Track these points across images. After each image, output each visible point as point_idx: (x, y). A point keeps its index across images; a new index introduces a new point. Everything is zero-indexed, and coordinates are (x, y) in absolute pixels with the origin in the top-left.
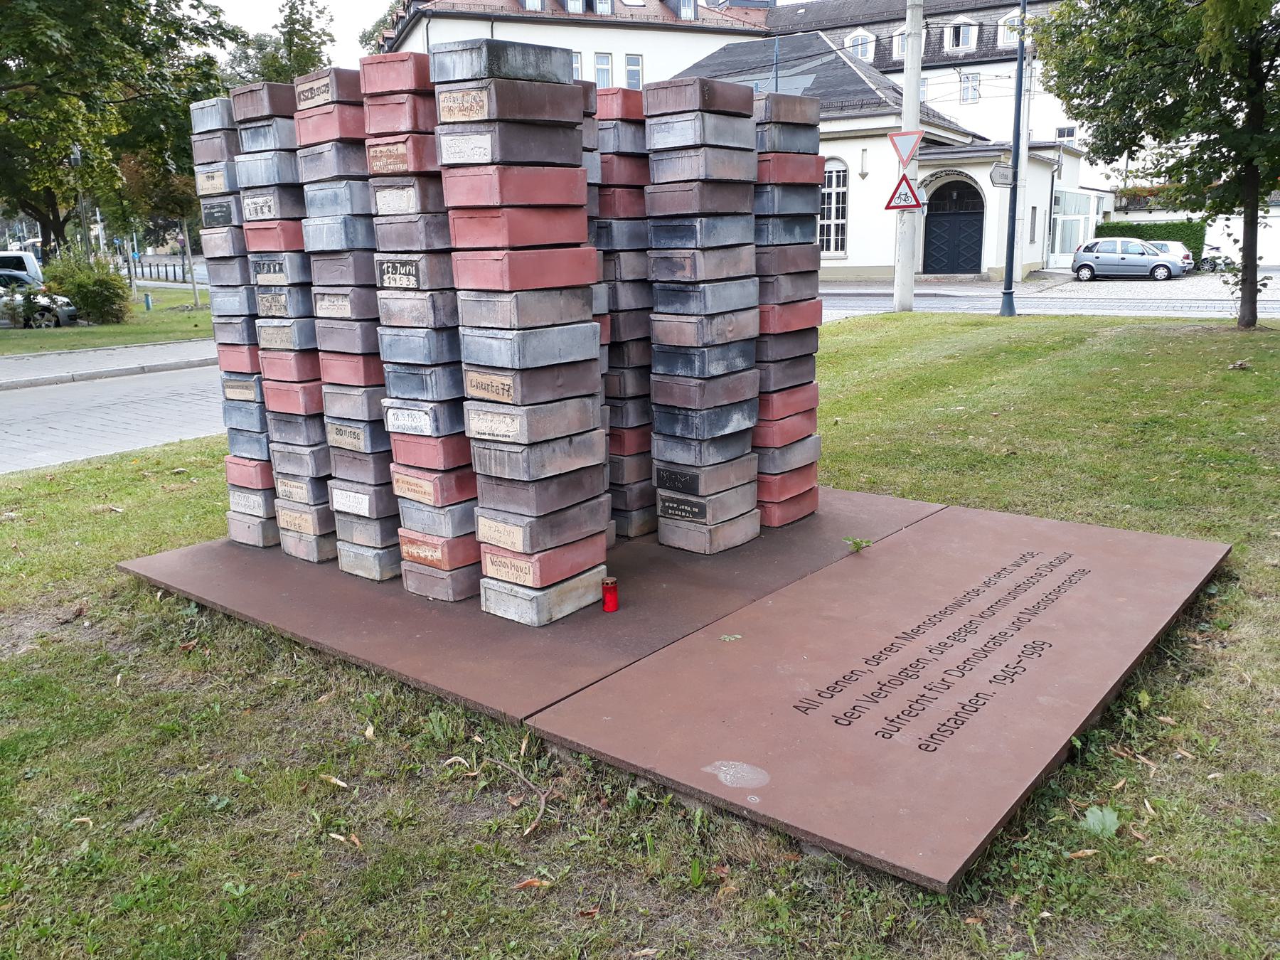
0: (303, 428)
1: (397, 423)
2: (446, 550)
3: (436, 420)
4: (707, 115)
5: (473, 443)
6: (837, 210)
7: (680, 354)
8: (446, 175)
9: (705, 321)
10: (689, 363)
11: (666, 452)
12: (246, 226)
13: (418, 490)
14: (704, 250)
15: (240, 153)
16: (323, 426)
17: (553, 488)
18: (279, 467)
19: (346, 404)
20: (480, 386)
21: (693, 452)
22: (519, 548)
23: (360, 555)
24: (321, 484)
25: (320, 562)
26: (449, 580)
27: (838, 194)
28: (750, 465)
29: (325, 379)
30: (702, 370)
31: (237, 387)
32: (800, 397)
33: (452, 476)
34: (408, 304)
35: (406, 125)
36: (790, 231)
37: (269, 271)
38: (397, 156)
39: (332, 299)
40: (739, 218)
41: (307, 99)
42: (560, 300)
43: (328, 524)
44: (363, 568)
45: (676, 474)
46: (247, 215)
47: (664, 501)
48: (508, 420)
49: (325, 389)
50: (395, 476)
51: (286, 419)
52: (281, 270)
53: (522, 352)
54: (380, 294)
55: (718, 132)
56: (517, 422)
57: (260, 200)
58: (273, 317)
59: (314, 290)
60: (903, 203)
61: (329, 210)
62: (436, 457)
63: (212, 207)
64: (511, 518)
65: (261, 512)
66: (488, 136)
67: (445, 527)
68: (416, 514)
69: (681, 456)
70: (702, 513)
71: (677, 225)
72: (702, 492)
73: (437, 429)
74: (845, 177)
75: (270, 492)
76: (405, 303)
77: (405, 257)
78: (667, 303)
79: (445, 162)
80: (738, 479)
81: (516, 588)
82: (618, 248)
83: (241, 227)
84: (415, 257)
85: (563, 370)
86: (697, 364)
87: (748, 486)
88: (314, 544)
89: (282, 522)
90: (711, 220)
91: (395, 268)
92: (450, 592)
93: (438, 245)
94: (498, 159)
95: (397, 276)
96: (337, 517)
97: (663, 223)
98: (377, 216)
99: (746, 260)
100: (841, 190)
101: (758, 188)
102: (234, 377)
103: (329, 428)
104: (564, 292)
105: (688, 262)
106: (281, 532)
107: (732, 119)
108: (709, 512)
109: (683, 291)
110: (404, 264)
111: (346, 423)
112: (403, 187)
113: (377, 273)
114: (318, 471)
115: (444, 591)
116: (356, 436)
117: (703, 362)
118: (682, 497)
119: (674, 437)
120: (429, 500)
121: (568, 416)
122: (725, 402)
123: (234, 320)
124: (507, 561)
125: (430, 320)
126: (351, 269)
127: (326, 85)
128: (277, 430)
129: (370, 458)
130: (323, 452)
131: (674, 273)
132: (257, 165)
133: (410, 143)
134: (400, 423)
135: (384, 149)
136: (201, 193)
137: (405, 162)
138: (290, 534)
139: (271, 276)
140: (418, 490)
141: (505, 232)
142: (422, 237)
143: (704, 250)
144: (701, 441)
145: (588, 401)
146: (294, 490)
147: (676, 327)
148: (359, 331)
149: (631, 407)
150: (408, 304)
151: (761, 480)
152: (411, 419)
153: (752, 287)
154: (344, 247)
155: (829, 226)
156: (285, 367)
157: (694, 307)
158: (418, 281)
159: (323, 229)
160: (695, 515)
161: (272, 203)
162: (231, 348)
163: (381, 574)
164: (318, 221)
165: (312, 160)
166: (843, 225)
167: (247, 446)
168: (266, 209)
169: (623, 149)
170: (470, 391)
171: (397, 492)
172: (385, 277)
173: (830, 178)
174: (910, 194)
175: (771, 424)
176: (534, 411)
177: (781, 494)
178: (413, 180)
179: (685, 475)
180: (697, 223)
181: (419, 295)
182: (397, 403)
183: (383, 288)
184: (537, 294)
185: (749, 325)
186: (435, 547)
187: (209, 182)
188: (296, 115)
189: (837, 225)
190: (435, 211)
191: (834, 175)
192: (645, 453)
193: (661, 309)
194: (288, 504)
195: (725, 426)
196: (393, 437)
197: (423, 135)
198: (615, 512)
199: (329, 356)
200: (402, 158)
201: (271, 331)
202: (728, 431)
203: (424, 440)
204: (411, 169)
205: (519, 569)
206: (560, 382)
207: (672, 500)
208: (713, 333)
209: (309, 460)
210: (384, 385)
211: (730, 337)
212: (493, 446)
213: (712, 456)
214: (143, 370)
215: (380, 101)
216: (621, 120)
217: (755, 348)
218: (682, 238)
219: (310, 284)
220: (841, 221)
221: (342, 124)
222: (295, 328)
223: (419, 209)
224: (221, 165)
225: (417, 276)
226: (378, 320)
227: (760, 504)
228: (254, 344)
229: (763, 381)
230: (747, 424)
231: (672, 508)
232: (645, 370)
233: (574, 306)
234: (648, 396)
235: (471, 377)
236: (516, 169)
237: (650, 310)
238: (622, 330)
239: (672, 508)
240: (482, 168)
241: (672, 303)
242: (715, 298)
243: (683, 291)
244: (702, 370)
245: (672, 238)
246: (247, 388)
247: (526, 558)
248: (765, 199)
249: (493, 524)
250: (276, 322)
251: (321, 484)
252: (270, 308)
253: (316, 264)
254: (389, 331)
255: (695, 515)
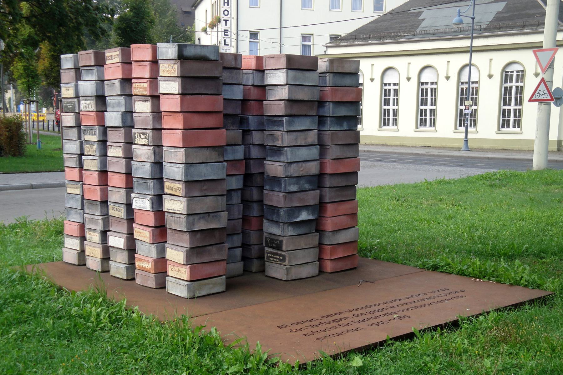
0: (99, 207)
1: (137, 205)
2: (153, 263)
3: (152, 203)
4: (289, 71)
5: (166, 214)
6: (516, 98)
7: (276, 180)
8: (161, 97)
9: (287, 165)
10: (280, 184)
11: (270, 229)
12: (81, 113)
13: (143, 235)
14: (287, 132)
15: (81, 80)
16: (108, 206)
17: (199, 235)
18: (88, 226)
19: (117, 196)
20: (170, 188)
21: (280, 229)
22: (182, 262)
23: (118, 268)
24: (104, 234)
25: (102, 272)
26: (154, 278)
27: (517, 87)
28: (314, 239)
29: (110, 184)
30: (285, 189)
31: (73, 188)
32: (345, 208)
33: (158, 229)
34: (144, 151)
35: (148, 76)
36: (341, 125)
37: (90, 134)
38: (144, 88)
39: (115, 148)
40: (308, 117)
41: (110, 59)
42: (207, 152)
43: (106, 250)
44: (119, 273)
45: (272, 239)
46: (82, 108)
47: (268, 253)
48: (179, 203)
49: (109, 189)
50: (135, 229)
51: (92, 202)
52: (95, 134)
53: (186, 173)
54: (134, 147)
55: (295, 78)
56: (183, 205)
57: (88, 102)
58: (90, 155)
59: (108, 144)
60: (541, 98)
61: (116, 109)
62: (151, 221)
63: (67, 103)
64: (179, 248)
65: (78, 248)
66: (177, 83)
67: (154, 254)
68: (142, 246)
69: (276, 230)
70: (284, 260)
71: (275, 120)
72: (284, 248)
73: (153, 207)
74: (522, 75)
75: (83, 238)
76: (143, 152)
77: (144, 131)
78: (271, 157)
79: (161, 92)
80: (306, 245)
81: (180, 281)
82: (252, 129)
83: (79, 113)
84: (148, 131)
85: (206, 183)
86: (283, 185)
87: (312, 249)
88: (100, 262)
89: (87, 253)
90: (291, 118)
91: (140, 136)
92: (154, 283)
93: (158, 127)
94: (180, 92)
95: (141, 139)
96: (111, 249)
97: (271, 118)
98: (135, 112)
99: (312, 137)
100: (520, 84)
101: (321, 103)
102: (71, 183)
103: (110, 207)
104: (209, 149)
105: (280, 137)
106: (86, 257)
107: (304, 72)
108: (287, 259)
109: (278, 150)
110: (144, 134)
111: (117, 205)
112: (146, 101)
113: (133, 137)
114: (104, 228)
115: (152, 284)
116: (120, 211)
117: (285, 185)
118: (276, 251)
119: (272, 221)
120: (148, 240)
121: (207, 204)
122: (298, 205)
123: (74, 156)
124: (177, 268)
125: (152, 159)
126: (123, 135)
127: (118, 55)
128: (89, 208)
129: (125, 221)
130: (106, 217)
131: (274, 142)
132: (88, 87)
133: (148, 83)
134: (138, 205)
135: (139, 84)
136: (63, 96)
137: (146, 91)
138: (90, 258)
139: (90, 136)
140: (143, 235)
141: (182, 122)
142: (151, 123)
143: (287, 132)
144: (285, 223)
145: (219, 198)
146: (93, 237)
147: (274, 168)
148: (124, 163)
149: (255, 206)
150: (144, 151)
151: (321, 246)
152: (142, 204)
153: (314, 152)
154: (121, 126)
155: (509, 110)
156: (92, 179)
157: (282, 158)
158: (148, 142)
159: (113, 118)
160: (281, 260)
161: (92, 104)
162: (71, 169)
163: (127, 276)
164: (111, 113)
165: (110, 86)
166: (520, 110)
167: (75, 216)
168: (90, 106)
169: (256, 84)
170: (167, 191)
171: (135, 237)
172: (136, 139)
173: (512, 76)
174: (546, 92)
175: (327, 219)
176: (190, 200)
177: (331, 255)
178: (149, 98)
179: (277, 240)
180: (284, 119)
181: (149, 148)
182: (137, 195)
183: (135, 144)
184: (195, 149)
185: (313, 168)
186: (148, 262)
187: (67, 91)
188: (105, 66)
189: (515, 110)
190: (157, 113)
191: (515, 74)
192: (261, 230)
193: (269, 158)
194: (90, 244)
195: (297, 217)
196: (135, 211)
197: (154, 79)
198: (244, 258)
199: (112, 174)
200: (145, 89)
201: (89, 161)
202: (298, 219)
203: (147, 212)
204: (148, 94)
205: (182, 272)
206: (205, 188)
207: (271, 253)
208: (294, 170)
209: (101, 222)
210: (132, 188)
211: (301, 173)
212: (173, 215)
213: (290, 231)
214: (32, 187)
215: (139, 64)
216: (255, 70)
217: (318, 180)
218: (278, 126)
219: (106, 141)
220: (518, 107)
221: (123, 72)
222: (99, 160)
223: (151, 111)
224: (73, 85)
225: (148, 139)
226: (132, 158)
227: (320, 259)
228: (81, 168)
229: (321, 197)
230: (311, 217)
231: (271, 257)
232: (261, 188)
233: (214, 156)
234: (262, 201)
235: (167, 184)
236: (188, 97)
237: (264, 159)
238: (252, 167)
239: (271, 257)
240: (174, 96)
241: (274, 156)
242: (289, 155)
243: (278, 150)
244: (285, 189)
245: (274, 126)
246: (77, 188)
247: (184, 266)
248: (326, 108)
249: (172, 251)
250: (91, 158)
251: (104, 234)
252: (89, 151)
253: (109, 131)
254: (136, 163)
255: (281, 260)
